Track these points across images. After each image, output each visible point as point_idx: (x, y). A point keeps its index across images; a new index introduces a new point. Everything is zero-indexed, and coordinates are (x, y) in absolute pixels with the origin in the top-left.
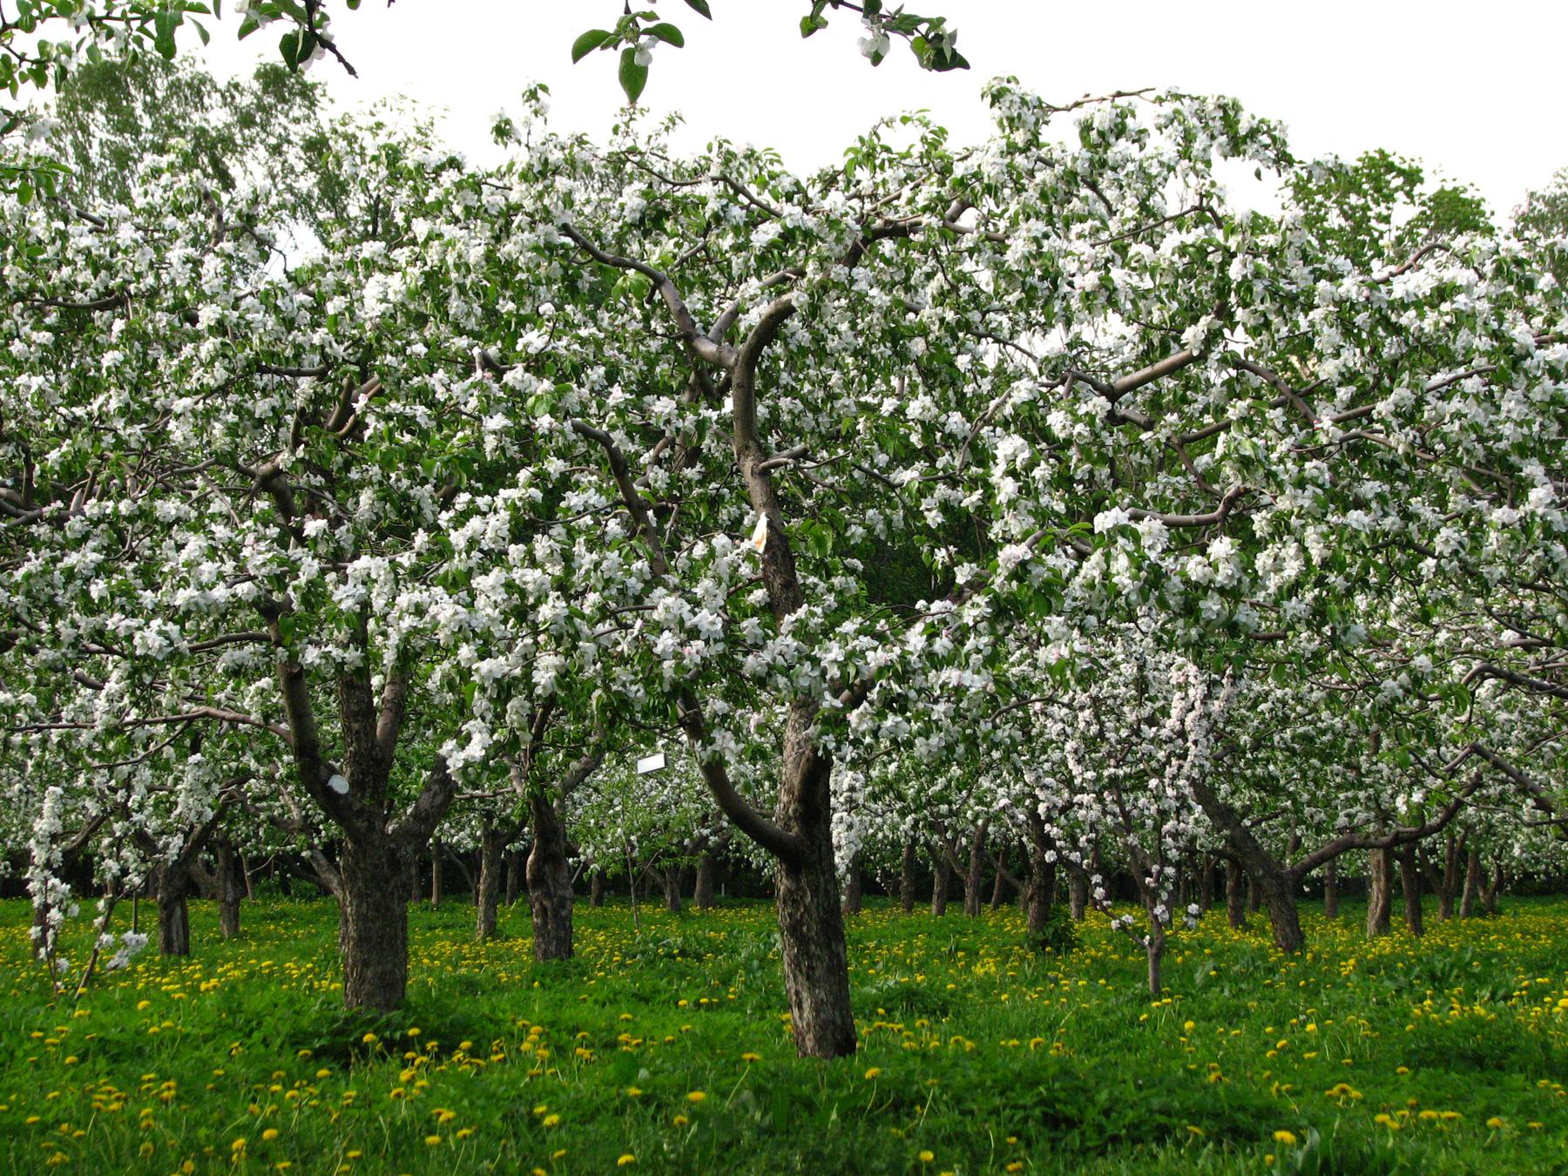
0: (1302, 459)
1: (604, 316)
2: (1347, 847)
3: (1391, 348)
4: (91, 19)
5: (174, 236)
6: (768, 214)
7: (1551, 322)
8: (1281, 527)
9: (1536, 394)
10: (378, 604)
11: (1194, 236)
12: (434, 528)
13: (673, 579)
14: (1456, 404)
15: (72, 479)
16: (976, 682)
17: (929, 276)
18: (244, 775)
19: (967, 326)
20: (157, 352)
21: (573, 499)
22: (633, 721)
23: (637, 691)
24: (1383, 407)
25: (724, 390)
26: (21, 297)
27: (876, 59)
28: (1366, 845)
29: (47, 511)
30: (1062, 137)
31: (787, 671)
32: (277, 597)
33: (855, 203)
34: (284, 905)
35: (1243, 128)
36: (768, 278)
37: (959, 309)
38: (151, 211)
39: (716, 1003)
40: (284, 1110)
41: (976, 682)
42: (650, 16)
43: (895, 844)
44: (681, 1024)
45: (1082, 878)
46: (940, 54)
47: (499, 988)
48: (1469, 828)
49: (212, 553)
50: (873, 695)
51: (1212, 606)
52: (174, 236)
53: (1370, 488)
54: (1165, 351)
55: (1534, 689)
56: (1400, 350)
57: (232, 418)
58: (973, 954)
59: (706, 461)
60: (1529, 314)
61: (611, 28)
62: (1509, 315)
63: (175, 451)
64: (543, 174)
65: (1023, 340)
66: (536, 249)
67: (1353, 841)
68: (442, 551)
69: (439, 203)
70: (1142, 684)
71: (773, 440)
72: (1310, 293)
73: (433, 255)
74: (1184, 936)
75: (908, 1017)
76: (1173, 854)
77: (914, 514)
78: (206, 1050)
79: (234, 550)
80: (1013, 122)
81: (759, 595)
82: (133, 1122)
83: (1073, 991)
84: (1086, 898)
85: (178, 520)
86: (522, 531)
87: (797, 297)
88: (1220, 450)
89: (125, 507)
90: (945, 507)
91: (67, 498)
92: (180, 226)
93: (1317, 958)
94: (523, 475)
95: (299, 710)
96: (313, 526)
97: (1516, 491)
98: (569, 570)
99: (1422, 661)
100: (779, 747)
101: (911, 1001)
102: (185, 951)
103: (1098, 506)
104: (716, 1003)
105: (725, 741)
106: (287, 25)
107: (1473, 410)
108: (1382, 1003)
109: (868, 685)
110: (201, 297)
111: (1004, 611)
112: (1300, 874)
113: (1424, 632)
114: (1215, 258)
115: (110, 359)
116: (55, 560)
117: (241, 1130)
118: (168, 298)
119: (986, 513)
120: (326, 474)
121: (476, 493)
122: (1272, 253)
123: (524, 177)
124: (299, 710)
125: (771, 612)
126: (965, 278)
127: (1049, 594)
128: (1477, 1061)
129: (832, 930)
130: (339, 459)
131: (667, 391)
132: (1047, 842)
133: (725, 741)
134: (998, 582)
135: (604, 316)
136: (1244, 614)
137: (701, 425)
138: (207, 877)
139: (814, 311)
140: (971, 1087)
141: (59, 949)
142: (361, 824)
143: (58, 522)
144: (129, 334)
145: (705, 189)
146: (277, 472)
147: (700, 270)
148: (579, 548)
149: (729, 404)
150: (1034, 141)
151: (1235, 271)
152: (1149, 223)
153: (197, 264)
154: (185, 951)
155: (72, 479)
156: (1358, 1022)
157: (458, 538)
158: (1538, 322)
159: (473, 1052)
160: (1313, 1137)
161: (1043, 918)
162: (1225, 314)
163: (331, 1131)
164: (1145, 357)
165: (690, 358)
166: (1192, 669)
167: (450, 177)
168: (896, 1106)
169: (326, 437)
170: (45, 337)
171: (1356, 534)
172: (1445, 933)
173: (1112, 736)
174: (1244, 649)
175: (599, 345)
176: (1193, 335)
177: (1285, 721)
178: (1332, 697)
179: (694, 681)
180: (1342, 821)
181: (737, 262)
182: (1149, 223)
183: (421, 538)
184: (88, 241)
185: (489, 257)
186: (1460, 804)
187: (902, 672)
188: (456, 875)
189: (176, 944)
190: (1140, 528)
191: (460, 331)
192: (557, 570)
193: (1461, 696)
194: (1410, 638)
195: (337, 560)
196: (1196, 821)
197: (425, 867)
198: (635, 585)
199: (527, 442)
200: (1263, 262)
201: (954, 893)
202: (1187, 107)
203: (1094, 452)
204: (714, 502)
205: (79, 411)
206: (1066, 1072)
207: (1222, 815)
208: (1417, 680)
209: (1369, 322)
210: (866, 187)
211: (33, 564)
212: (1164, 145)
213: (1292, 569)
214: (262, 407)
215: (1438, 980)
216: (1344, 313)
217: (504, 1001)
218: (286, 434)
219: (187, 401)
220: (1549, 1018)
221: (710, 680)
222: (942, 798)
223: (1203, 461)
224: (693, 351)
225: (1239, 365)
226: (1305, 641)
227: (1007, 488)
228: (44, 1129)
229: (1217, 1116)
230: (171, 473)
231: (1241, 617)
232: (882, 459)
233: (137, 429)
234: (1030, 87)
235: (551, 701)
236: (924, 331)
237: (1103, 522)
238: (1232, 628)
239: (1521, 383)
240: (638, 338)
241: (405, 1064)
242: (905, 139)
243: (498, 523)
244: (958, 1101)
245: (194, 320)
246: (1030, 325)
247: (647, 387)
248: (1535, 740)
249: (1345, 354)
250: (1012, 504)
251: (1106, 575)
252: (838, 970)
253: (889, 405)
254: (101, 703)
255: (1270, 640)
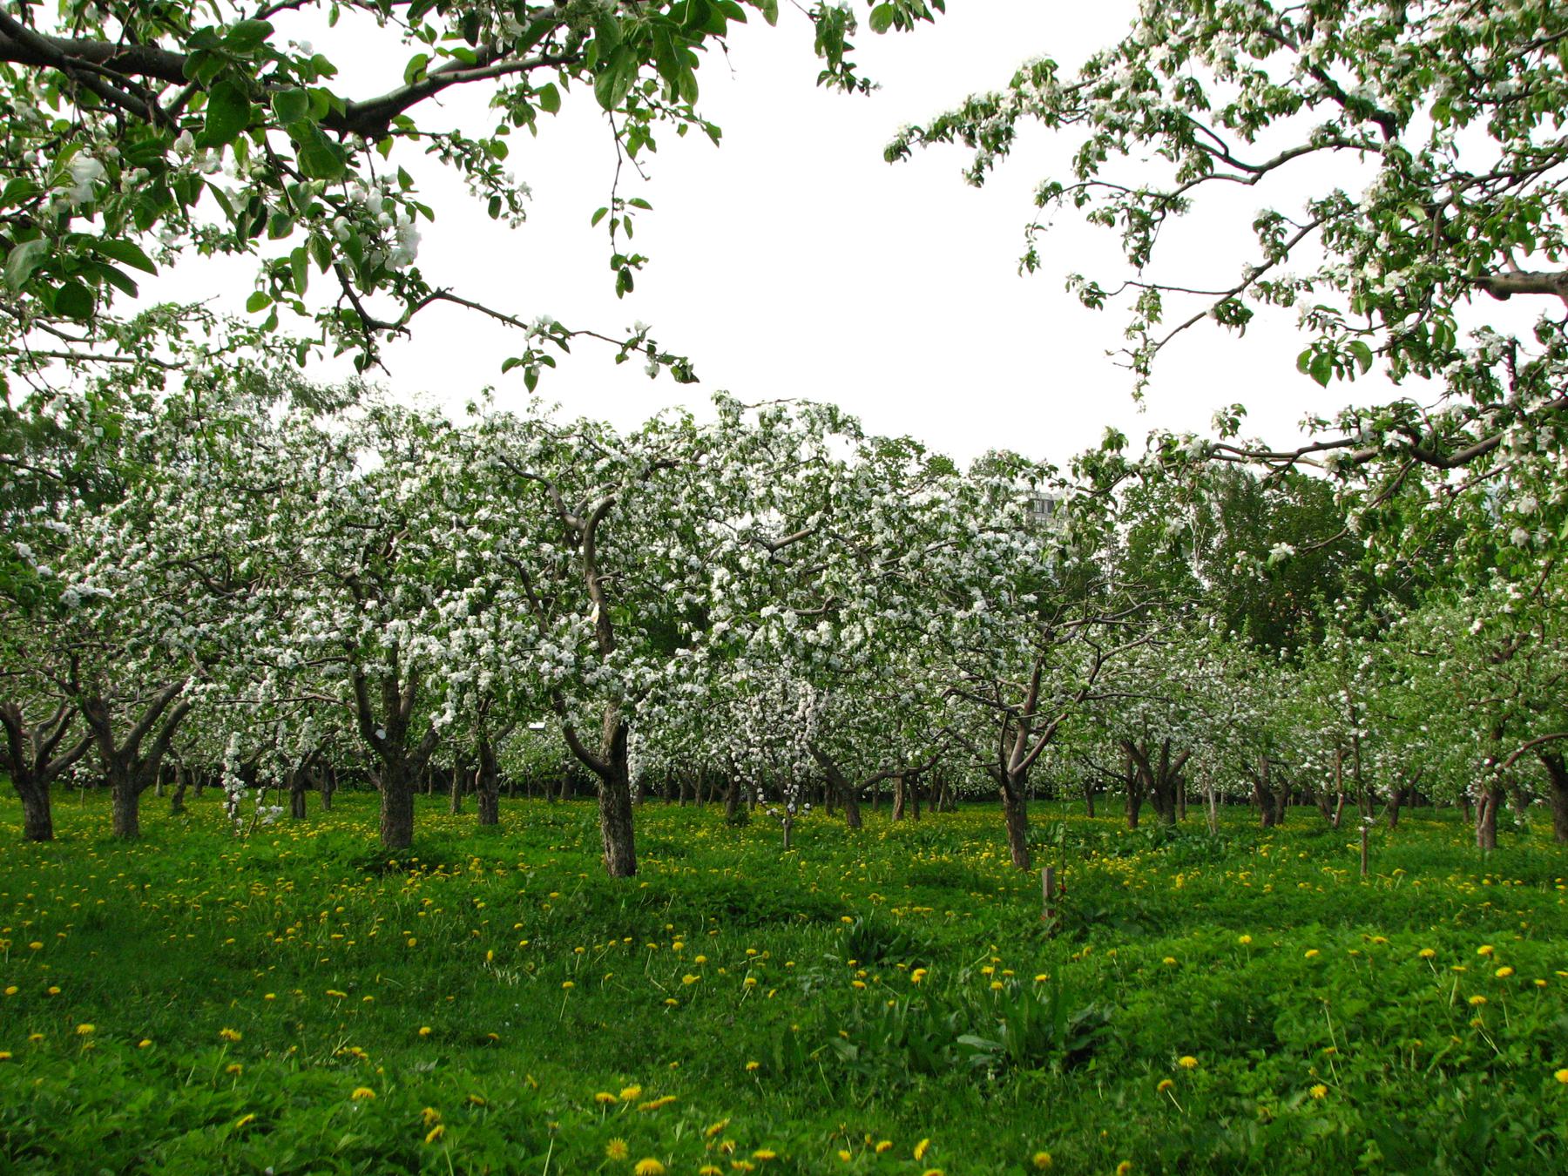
0: (864, 584)
1: (521, 503)
2: (884, 776)
3: (909, 531)
4: (265, 347)
5: (306, 456)
6: (605, 454)
7: (987, 520)
8: (853, 617)
9: (978, 556)
10: (402, 643)
11: (813, 472)
12: (431, 607)
13: (550, 635)
14: (939, 559)
15: (251, 578)
16: (700, 690)
17: (683, 487)
18: (334, 729)
19: (701, 513)
20: (296, 515)
21: (501, 594)
22: (532, 708)
23: (531, 691)
24: (904, 559)
25: (580, 542)
26: (227, 485)
27: (653, 376)
28: (893, 776)
29: (238, 593)
30: (750, 422)
31: (606, 683)
32: (351, 639)
33: (649, 451)
34: (354, 794)
35: (839, 419)
36: (603, 486)
37: (698, 504)
38: (294, 444)
39: (564, 851)
40: (348, 896)
41: (700, 690)
42: (540, 352)
43: (661, 771)
44: (550, 859)
45: (753, 789)
46: (685, 374)
47: (460, 839)
48: (943, 768)
49: (318, 616)
50: (649, 696)
51: (818, 655)
52: (306, 456)
53: (897, 599)
54: (799, 528)
55: (975, 700)
56: (913, 531)
57: (333, 548)
58: (698, 827)
59: (570, 577)
60: (976, 516)
61: (520, 357)
62: (966, 516)
63: (304, 565)
64: (491, 431)
65: (730, 521)
66: (487, 468)
67: (887, 773)
68: (434, 618)
69: (439, 444)
70: (785, 694)
71: (604, 567)
72: (870, 502)
73: (435, 470)
74: (803, 820)
75: (664, 858)
76: (798, 778)
77: (673, 606)
78: (310, 867)
79: (330, 617)
80: (726, 413)
81: (594, 644)
82: (272, 902)
83: (747, 845)
84: (755, 799)
85: (304, 600)
86: (475, 609)
87: (617, 496)
88: (823, 578)
89: (277, 592)
90: (688, 603)
91: (249, 587)
92: (309, 451)
93: (867, 831)
94: (477, 581)
95: (362, 698)
96: (371, 604)
97: (967, 603)
98: (498, 630)
99: (921, 686)
100: (602, 721)
101: (667, 849)
102: (303, 816)
103: (763, 604)
104: (564, 851)
105: (574, 718)
106: (358, 351)
107: (948, 562)
108: (898, 854)
109: (646, 691)
110: (319, 487)
111: (715, 655)
112: (861, 789)
113: (923, 672)
114: (823, 483)
115: (273, 518)
116: (241, 618)
117: (326, 907)
118: (302, 488)
119: (706, 608)
120: (379, 578)
121: (453, 590)
122: (852, 481)
123: (481, 432)
124: (362, 698)
125: (599, 652)
126: (701, 489)
127: (738, 647)
128: (943, 883)
129: (626, 812)
130: (385, 571)
131: (550, 541)
132: (736, 772)
133: (574, 718)
134: (712, 640)
135: (521, 503)
136: (834, 660)
137: (566, 558)
138: (314, 779)
139: (626, 503)
140: (693, 893)
141: (238, 814)
142: (391, 755)
143: (243, 599)
144: (282, 506)
145: (573, 441)
146: (354, 576)
147: (568, 481)
148: (504, 618)
149: (581, 550)
150: (736, 423)
151: (833, 490)
152: (792, 464)
153: (317, 471)
154: (303, 816)
155: (251, 578)
156: (886, 863)
157: (442, 612)
158: (980, 520)
159: (444, 871)
160: (860, 920)
161: (733, 809)
162: (828, 510)
163: (373, 908)
164: (788, 531)
165: (563, 525)
166: (809, 687)
167: (444, 431)
168: (656, 901)
169: (381, 559)
170: (239, 506)
171: (890, 621)
172: (931, 820)
173: (769, 719)
174: (835, 678)
175: (517, 517)
176: (812, 520)
177: (855, 714)
178: (877, 702)
179: (561, 686)
180: (881, 763)
181: (588, 478)
182: (792, 464)
183: (424, 612)
184: (262, 457)
185: (463, 471)
186: (938, 756)
187: (664, 685)
188: (441, 781)
189: (299, 813)
190: (784, 616)
191: (448, 508)
192: (492, 629)
193: (938, 703)
194: (917, 673)
195: (382, 622)
196: (810, 762)
197: (425, 778)
198: (531, 637)
199: (480, 566)
200: (847, 486)
201: (690, 796)
202: (811, 408)
203: (762, 577)
204: (573, 598)
205: (255, 543)
206: (740, 886)
207: (822, 759)
208: (918, 695)
209: (898, 517)
210: (654, 442)
211: (230, 621)
212: (800, 426)
213: (858, 638)
214: (348, 543)
215: (925, 843)
216: (886, 511)
217: (459, 846)
218: (360, 557)
219: (311, 540)
220: (978, 862)
221: (570, 687)
222: (685, 748)
223: (816, 584)
224: (565, 522)
225: (835, 536)
226: (865, 675)
227: (718, 594)
228: (227, 904)
229: (814, 908)
230: (301, 574)
231: (832, 662)
232: (658, 578)
233: (285, 553)
234: (735, 395)
235: (489, 695)
236: (679, 515)
237: (765, 612)
238: (829, 666)
239: (971, 550)
240: (537, 515)
241: (410, 876)
242: (673, 419)
243: (463, 604)
244: (687, 899)
245: (314, 499)
246: (733, 514)
247: (542, 538)
248: (976, 726)
249: (886, 532)
250: (721, 602)
251: (766, 639)
252: (629, 834)
253: (660, 552)
254: (262, 689)
255: (848, 673)
